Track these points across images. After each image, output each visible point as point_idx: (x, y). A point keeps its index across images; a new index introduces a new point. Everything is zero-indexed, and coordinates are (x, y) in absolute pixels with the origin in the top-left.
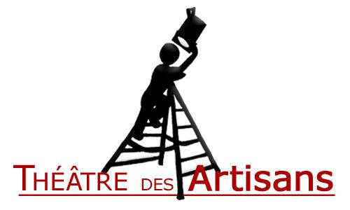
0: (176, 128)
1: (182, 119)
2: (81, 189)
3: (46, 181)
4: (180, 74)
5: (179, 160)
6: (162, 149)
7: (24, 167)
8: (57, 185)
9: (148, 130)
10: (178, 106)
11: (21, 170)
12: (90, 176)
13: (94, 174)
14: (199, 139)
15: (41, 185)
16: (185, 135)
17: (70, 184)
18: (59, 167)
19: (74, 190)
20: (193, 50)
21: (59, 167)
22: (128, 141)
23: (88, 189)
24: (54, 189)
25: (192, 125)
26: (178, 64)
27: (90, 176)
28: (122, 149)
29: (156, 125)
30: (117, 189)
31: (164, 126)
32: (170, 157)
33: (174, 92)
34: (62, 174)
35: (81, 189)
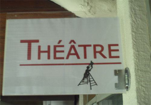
0: (90, 79)
1: (91, 77)
2: (78, 58)
3: (48, 52)
4: (90, 70)
5: (90, 84)
6: (88, 82)
7: (30, 42)
8: (58, 55)
9: (85, 79)
10: (90, 75)
11: (26, 45)
12: (87, 48)
13: (90, 46)
14: (94, 80)
15: (44, 56)
16: (91, 80)
17: (69, 54)
18: (60, 41)
19: (73, 59)
20: (92, 67)
21: (60, 41)
22: (82, 81)
23: (85, 57)
24: (55, 58)
25: (93, 78)
26: (89, 69)
27: (87, 48)
28: (81, 82)
29: (86, 78)
30: (111, 57)
31: (88, 78)
32: (89, 83)
33: (89, 73)
34: (63, 46)
35: (78, 58)
